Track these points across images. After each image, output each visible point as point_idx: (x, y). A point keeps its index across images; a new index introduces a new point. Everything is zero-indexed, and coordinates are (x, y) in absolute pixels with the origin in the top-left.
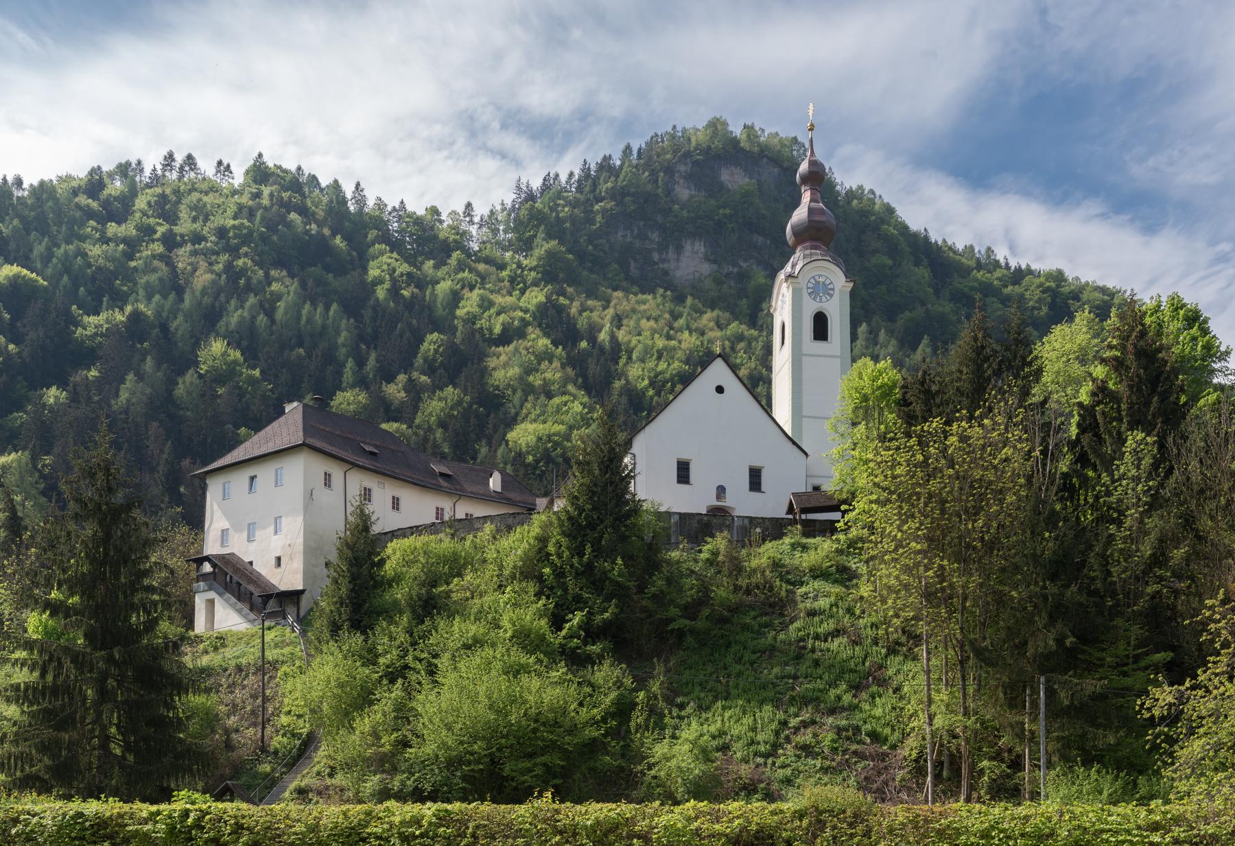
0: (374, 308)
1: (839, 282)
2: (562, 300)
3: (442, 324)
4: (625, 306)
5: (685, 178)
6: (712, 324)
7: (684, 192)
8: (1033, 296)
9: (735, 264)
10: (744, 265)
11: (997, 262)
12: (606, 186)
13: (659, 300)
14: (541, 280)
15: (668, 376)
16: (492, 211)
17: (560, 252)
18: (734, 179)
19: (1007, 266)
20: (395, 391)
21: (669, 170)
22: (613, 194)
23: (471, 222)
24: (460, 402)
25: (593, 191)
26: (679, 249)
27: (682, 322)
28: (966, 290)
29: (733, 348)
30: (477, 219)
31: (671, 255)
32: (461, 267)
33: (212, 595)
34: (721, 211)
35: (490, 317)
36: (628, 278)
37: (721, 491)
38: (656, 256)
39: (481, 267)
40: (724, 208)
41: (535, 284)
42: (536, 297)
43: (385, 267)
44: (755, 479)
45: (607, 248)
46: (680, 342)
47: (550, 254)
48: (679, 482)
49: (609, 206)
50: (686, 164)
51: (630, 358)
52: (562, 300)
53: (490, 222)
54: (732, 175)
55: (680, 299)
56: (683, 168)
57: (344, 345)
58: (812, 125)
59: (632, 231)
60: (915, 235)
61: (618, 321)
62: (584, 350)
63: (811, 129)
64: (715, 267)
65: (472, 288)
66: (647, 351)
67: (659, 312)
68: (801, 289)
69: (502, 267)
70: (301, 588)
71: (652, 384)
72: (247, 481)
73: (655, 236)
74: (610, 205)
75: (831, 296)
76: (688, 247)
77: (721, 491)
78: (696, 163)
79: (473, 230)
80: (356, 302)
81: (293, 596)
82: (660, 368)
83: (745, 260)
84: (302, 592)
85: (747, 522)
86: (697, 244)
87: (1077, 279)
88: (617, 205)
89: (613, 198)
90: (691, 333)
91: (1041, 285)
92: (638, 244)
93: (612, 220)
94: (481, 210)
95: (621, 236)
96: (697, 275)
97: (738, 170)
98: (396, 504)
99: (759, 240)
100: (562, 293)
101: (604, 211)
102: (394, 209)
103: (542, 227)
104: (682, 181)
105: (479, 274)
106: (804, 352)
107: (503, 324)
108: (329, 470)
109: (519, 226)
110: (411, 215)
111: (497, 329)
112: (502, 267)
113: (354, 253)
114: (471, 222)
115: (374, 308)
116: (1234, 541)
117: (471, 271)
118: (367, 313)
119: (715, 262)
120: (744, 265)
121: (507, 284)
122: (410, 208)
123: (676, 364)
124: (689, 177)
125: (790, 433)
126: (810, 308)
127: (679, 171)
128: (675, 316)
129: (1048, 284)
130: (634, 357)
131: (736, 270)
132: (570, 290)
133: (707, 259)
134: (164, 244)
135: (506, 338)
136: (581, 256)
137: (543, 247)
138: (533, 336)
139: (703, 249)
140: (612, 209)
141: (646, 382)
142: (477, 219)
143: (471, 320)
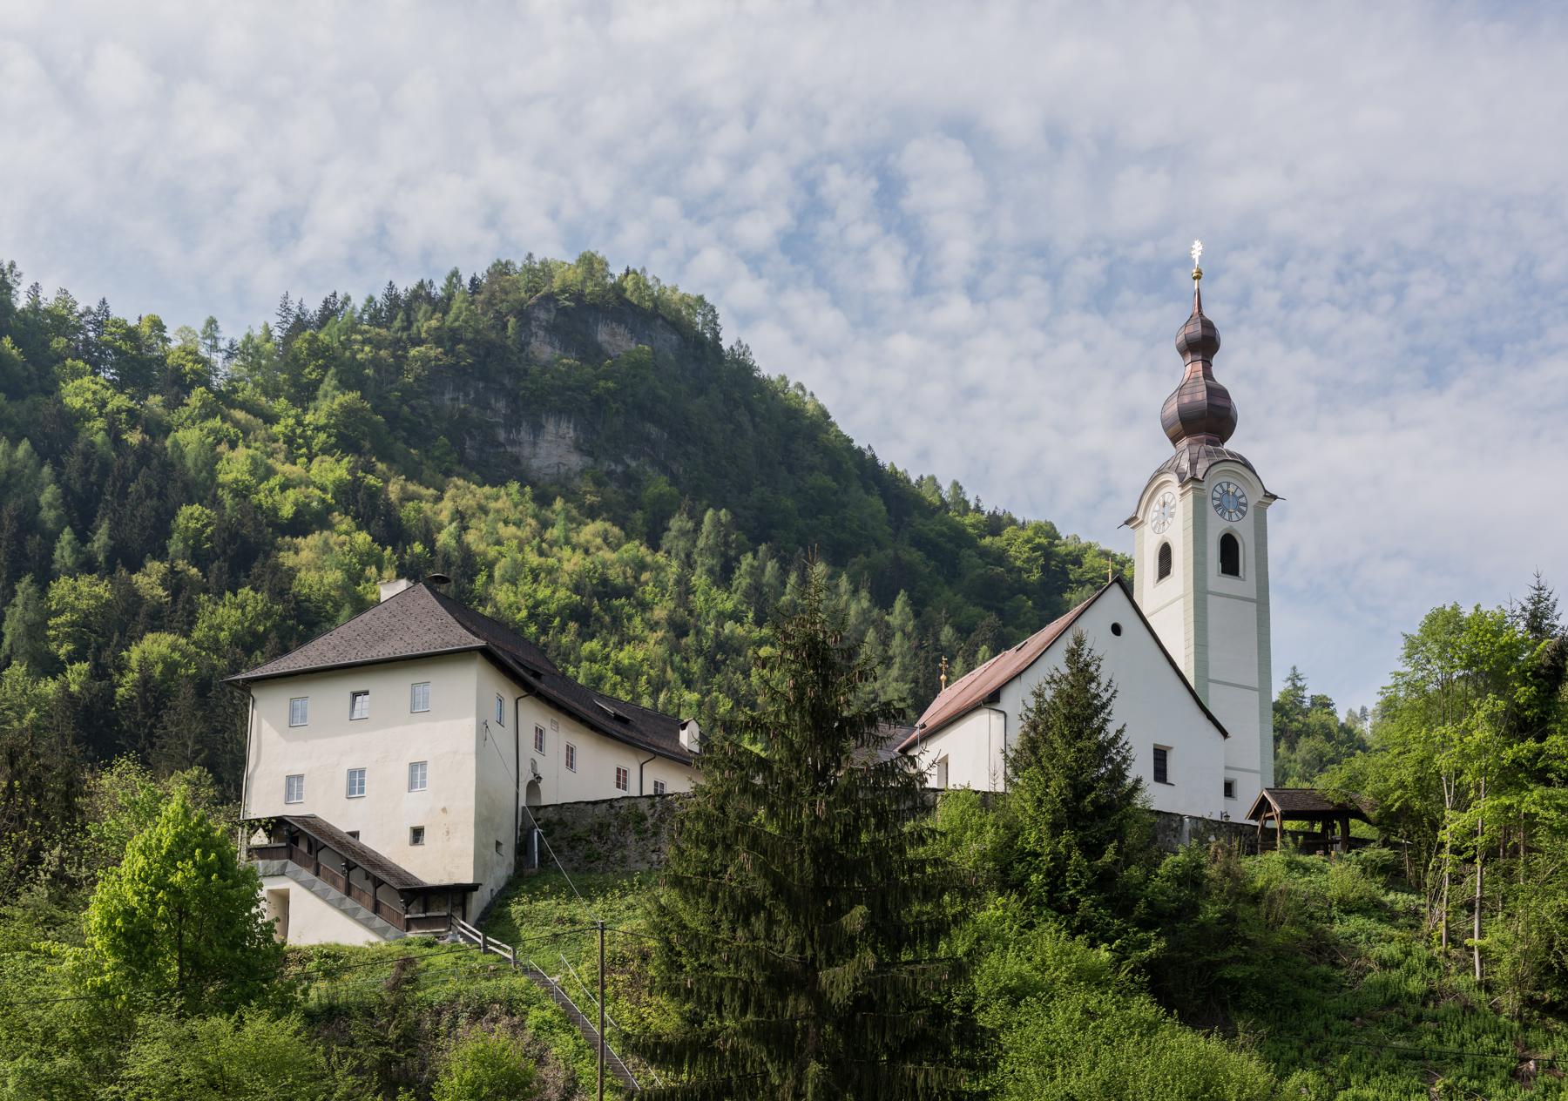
0: (86, 456)
2: (371, 480)
3: (202, 489)
4: (467, 502)
5: (546, 329)
6: (599, 541)
7: (544, 350)
8: (1019, 553)
9: (618, 460)
10: (633, 464)
11: (966, 503)
12: (426, 324)
13: (516, 497)
14: (335, 446)
15: (553, 607)
16: (248, 336)
17: (363, 409)
18: (615, 341)
19: (978, 510)
20: (149, 581)
21: (523, 315)
22: (438, 338)
23: (214, 348)
24: (267, 614)
25: (407, 328)
26: (537, 429)
27: (553, 533)
28: (932, 535)
29: (637, 579)
30: (223, 345)
31: (525, 435)
32: (208, 412)
34: (602, 383)
35: (271, 490)
36: (462, 460)
38: (502, 435)
39: (239, 415)
40: (606, 379)
41: (326, 450)
42: (332, 470)
43: (89, 395)
45: (429, 413)
46: (559, 560)
47: (348, 411)
49: (432, 353)
50: (548, 311)
51: (490, 577)
52: (371, 480)
53: (249, 352)
54: (613, 335)
55: (543, 500)
56: (543, 315)
57: (50, 506)
58: (1199, 272)
59: (467, 395)
60: (860, 452)
61: (460, 516)
62: (418, 556)
63: (1198, 278)
64: (590, 461)
65: (233, 446)
66: (518, 567)
67: (518, 516)
68: (1205, 498)
69: (271, 419)
70: (467, 878)
71: (532, 616)
72: (348, 697)
73: (501, 405)
74: (435, 352)
75: (1244, 513)
76: (550, 427)
78: (563, 311)
79: (218, 359)
80: (56, 436)
81: (456, 895)
82: (540, 596)
83: (634, 457)
84: (474, 887)
85: (1200, 824)
86: (564, 425)
87: (1076, 538)
88: (445, 354)
89: (439, 342)
90: (574, 550)
91: (1029, 541)
92: (475, 412)
93: (434, 377)
94: (231, 334)
95: (450, 400)
96: (563, 470)
97: (621, 330)
99: (653, 430)
100: (370, 469)
101: (425, 360)
102: (88, 311)
103: (332, 370)
104: (541, 333)
105: (236, 424)
107: (296, 504)
109: (293, 363)
110: (119, 324)
111: (287, 511)
112: (271, 419)
113: (32, 368)
114: (214, 348)
115: (86, 456)
117: (224, 420)
118: (74, 463)
119: (590, 454)
120: (633, 464)
121: (281, 444)
122: (116, 313)
123: (562, 594)
124: (552, 329)
126: (1217, 527)
127: (537, 319)
128: (545, 524)
129: (1037, 540)
130: (497, 574)
131: (620, 469)
132: (381, 466)
133: (577, 448)
135: (302, 524)
136: (393, 419)
137: (331, 401)
138: (344, 527)
139: (572, 434)
140: (437, 359)
141: (524, 613)
142: (223, 345)
143: (242, 492)
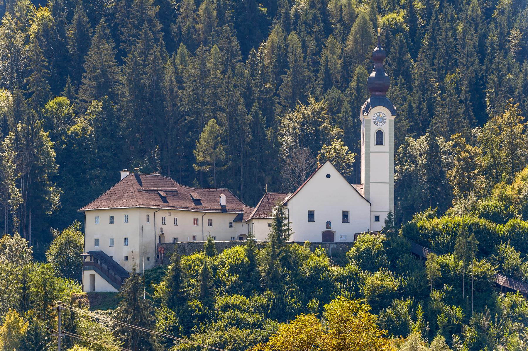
1: (390, 117)
33: (93, 272)
37: (329, 224)
44: (345, 216)
48: (309, 221)
75: (385, 122)
77: (329, 224)
98: (176, 222)
106: (371, 151)
108: (148, 214)
116: (475, 4)
125: (363, 196)
131: (459, 234)
134: (443, 287)
